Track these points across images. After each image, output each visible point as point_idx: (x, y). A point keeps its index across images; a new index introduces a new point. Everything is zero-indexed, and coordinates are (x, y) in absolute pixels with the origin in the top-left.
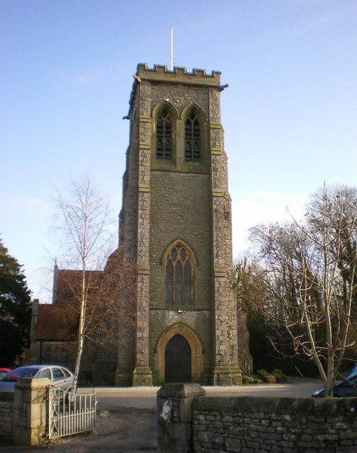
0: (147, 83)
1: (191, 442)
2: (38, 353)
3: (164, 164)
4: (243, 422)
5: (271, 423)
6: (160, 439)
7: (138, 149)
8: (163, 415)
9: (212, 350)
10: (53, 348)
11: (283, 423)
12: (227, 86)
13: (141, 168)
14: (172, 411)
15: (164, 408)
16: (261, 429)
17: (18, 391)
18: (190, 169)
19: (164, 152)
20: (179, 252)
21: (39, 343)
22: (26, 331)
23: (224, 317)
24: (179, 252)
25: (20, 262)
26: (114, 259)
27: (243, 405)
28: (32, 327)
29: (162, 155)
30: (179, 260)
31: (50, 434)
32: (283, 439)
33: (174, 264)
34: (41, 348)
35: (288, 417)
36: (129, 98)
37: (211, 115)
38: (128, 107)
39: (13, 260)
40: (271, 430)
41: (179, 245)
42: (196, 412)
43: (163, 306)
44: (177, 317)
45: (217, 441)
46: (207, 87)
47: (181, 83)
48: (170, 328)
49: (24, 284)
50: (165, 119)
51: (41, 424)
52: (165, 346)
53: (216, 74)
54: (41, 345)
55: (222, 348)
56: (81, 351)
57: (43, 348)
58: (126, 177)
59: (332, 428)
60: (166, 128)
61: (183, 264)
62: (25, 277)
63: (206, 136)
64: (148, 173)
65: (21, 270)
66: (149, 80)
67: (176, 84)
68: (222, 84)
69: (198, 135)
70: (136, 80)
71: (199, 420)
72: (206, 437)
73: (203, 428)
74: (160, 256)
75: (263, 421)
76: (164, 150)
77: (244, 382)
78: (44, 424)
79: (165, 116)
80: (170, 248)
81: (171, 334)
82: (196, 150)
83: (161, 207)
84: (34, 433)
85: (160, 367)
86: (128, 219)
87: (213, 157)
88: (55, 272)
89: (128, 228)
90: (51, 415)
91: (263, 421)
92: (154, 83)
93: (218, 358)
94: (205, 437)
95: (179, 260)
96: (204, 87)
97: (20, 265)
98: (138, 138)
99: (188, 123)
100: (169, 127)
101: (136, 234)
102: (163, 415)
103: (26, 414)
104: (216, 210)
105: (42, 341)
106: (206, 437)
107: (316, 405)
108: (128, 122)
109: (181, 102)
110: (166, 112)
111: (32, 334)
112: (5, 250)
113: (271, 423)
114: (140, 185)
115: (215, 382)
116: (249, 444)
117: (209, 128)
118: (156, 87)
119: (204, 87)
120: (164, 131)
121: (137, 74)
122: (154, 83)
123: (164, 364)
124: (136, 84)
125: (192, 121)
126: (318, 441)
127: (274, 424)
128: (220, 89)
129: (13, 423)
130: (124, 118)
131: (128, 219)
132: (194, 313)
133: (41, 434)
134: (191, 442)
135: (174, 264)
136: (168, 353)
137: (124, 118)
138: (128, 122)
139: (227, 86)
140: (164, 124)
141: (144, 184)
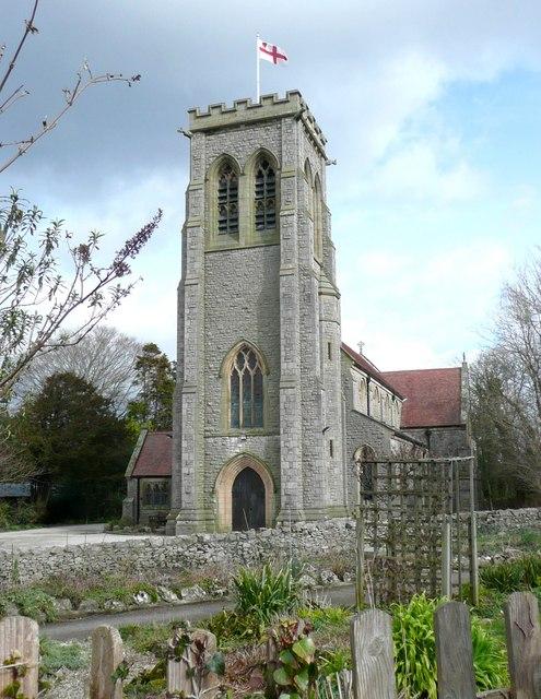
10: (152, 486)
18: (256, 243)
20: (246, 357)
23: (292, 444)
24: (246, 357)
33: (241, 374)
34: (138, 487)
37: (285, 159)
38: (328, 204)
41: (246, 349)
47: (242, 123)
50: (228, 178)
55: (291, 485)
57: (141, 486)
60: (231, 189)
61: (252, 373)
64: (201, 259)
67: (235, 126)
69: (274, 190)
82: (270, 212)
85: (222, 511)
100: (235, 188)
109: (242, 147)
110: (227, 167)
115: (127, 512)
118: (212, 137)
125: (265, 172)
132: (263, 439)
135: (241, 374)
140: (229, 184)
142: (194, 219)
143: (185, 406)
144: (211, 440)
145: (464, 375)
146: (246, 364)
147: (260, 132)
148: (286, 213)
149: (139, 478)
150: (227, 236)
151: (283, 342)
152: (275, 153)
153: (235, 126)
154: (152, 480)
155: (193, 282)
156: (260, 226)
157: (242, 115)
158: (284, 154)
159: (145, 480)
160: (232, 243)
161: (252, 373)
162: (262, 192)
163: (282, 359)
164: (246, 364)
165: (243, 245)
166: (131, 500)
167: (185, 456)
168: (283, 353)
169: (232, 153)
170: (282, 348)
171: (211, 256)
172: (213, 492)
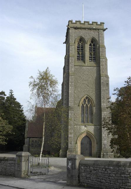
0: (72, 28)
1: (79, 176)
2: (28, 143)
3: (81, 63)
4: (97, 169)
5: (106, 170)
6: (67, 175)
7: (69, 57)
8: (69, 166)
9: (101, 143)
11: (110, 169)
12: (107, 29)
13: (70, 65)
14: (72, 165)
15: (69, 163)
16: (102, 172)
17: (17, 157)
19: (81, 58)
20: (87, 101)
21: (28, 139)
22: (23, 133)
24: (87, 101)
25: (21, 104)
26: (60, 104)
27: (110, 163)
28: (26, 132)
29: (79, 59)
30: (87, 104)
31: (29, 174)
32: (110, 176)
33: (85, 106)
35: (112, 168)
36: (65, 35)
37: (100, 42)
39: (18, 103)
40: (106, 172)
41: (87, 98)
42: (81, 165)
43: (80, 123)
44: (86, 128)
45: (88, 176)
46: (98, 29)
48: (82, 133)
49: (23, 114)
51: (26, 169)
52: (81, 141)
53: (102, 24)
54: (29, 139)
55: (105, 142)
56: (43, 142)
57: (30, 141)
58: (64, 68)
59: (127, 172)
62: (23, 111)
63: (98, 51)
65: (22, 108)
66: (73, 27)
67: (85, 29)
68: (105, 28)
70: (68, 27)
71: (81, 168)
72: (84, 175)
73: (83, 171)
74: (78, 103)
75: (103, 169)
76: (81, 57)
77: (115, 157)
78: (27, 170)
79: (80, 42)
80: (83, 99)
81: (83, 135)
83: (79, 81)
84: (23, 173)
85: (78, 150)
86: (65, 87)
87: (101, 60)
88: (36, 108)
89: (65, 91)
90: (29, 168)
91: (103, 169)
92: (76, 28)
93: (103, 146)
94: (84, 174)
95: (87, 104)
96: (99, 28)
97: (21, 106)
98: (69, 52)
99: (90, 45)
101: (68, 93)
102: (69, 166)
103: (20, 165)
104: (102, 82)
105: (30, 138)
106: (84, 175)
107: (121, 163)
108: (65, 45)
111: (25, 135)
112: (15, 99)
113: (106, 170)
114: (70, 72)
115: (102, 157)
116: (99, 177)
117: (99, 47)
118: (76, 30)
119: (99, 28)
120: (81, 49)
121: (68, 25)
122: (76, 28)
123: (80, 148)
124: (68, 29)
126: (122, 177)
127: (107, 170)
128: (104, 30)
129: (15, 169)
130: (64, 43)
131: (65, 87)
133: (26, 174)
134: (79, 176)
135: (85, 106)
136: (82, 144)
137: (64, 43)
138: (65, 45)
139: (107, 29)
141: (72, 70)
142: (72, 54)
143: (70, 114)
144: (75, 126)
145: (112, 108)
146: (87, 103)
147: (92, 32)
148: (102, 58)
149: (30, 138)
150: (92, 62)
151: (102, 97)
152: (97, 39)
153: (85, 29)
154: (34, 139)
155: (72, 74)
156: (90, 60)
157: (86, 26)
158: (100, 40)
159: (32, 139)
160: (83, 64)
161: (89, 106)
162: (91, 50)
163: (102, 102)
164: (87, 103)
165: (86, 65)
166: (27, 145)
167: (70, 131)
168: (102, 100)
169: (83, 36)
170: (102, 99)
171: (76, 67)
172: (76, 143)
